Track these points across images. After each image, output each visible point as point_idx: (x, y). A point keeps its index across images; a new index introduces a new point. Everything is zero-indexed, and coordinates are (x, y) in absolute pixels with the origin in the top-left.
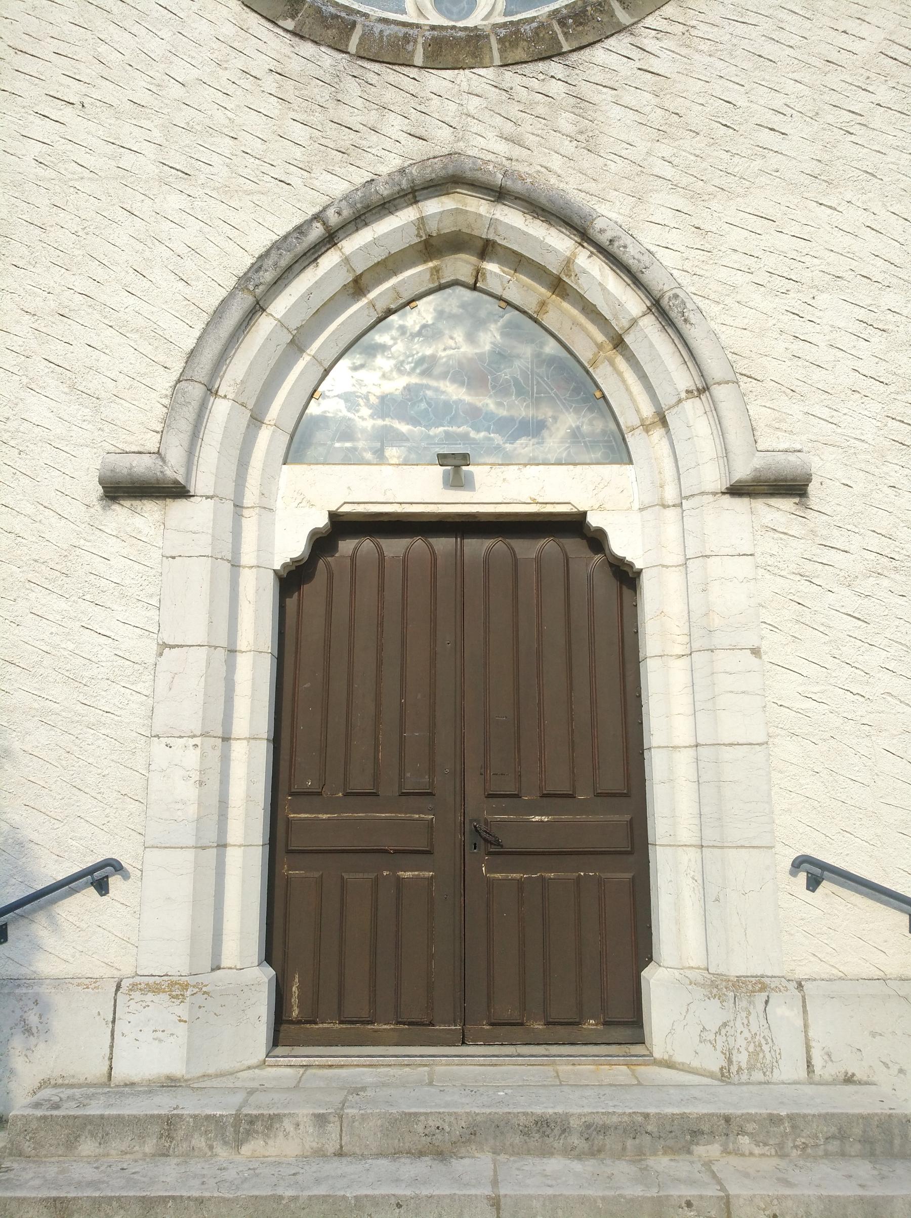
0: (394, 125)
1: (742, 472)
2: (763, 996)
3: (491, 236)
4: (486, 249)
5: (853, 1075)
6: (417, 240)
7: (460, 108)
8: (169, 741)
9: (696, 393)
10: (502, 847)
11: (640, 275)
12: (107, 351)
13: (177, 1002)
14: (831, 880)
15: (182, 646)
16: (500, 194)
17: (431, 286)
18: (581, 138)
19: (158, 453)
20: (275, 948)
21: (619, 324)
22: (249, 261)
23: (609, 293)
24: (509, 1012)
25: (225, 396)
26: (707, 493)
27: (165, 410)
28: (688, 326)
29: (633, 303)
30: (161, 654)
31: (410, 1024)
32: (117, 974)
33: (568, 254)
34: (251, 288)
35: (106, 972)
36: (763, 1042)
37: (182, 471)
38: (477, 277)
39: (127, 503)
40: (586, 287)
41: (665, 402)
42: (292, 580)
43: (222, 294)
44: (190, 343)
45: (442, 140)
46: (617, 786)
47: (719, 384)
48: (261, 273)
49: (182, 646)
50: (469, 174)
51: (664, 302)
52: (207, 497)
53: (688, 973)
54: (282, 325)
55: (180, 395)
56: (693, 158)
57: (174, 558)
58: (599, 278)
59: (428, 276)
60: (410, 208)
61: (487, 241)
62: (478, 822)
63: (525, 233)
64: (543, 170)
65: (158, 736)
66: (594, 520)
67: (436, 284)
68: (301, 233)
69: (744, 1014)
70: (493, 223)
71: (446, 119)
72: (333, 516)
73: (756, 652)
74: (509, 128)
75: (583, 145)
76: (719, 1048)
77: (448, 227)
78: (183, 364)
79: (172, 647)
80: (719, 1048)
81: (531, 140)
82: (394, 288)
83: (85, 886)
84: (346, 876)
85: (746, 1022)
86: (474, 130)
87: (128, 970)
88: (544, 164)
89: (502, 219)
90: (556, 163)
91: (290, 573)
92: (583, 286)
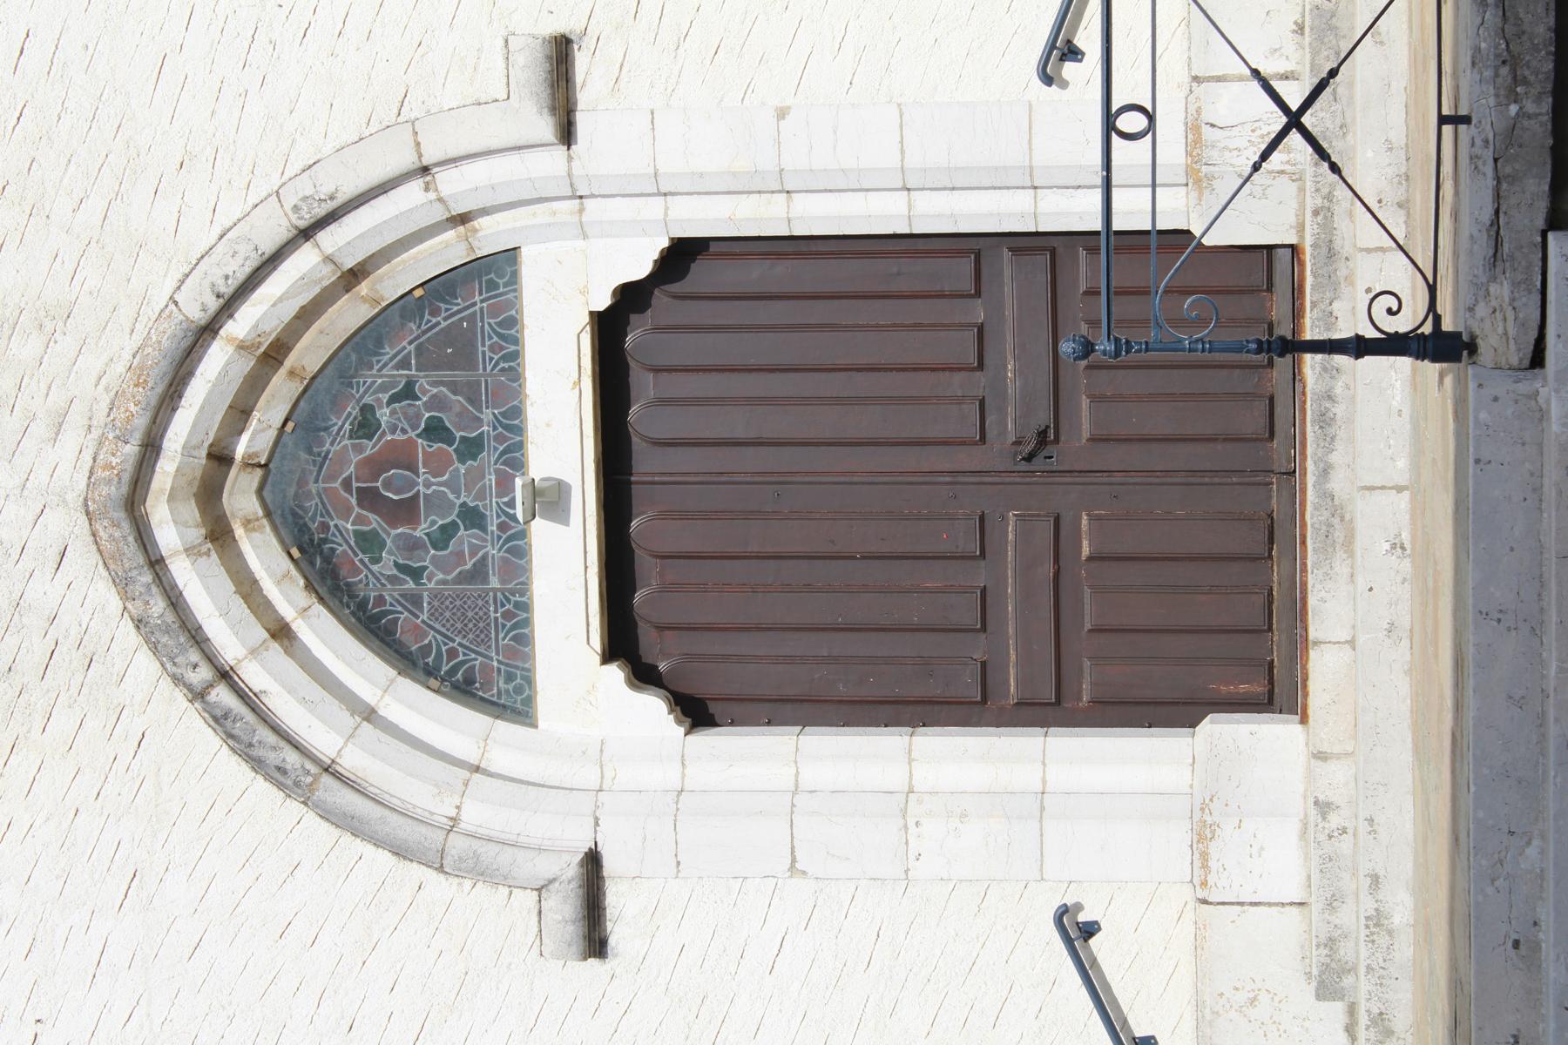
0: (44, 591)
1: (544, 127)
2: (1206, 129)
3: (204, 453)
4: (220, 458)
5: (1296, 23)
6: (214, 555)
7: (12, 498)
8: (912, 857)
9: (429, 178)
10: (1048, 427)
11: (266, 256)
12: (399, 966)
13: (1218, 832)
14: (1074, 27)
15: (793, 848)
16: (151, 447)
17: (268, 529)
18: (49, 326)
19: (539, 890)
20: (1181, 711)
21: (328, 276)
22: (261, 784)
23: (287, 292)
24: (1253, 421)
25: (458, 807)
26: (570, 168)
27: (480, 884)
28: (339, 195)
29: (304, 260)
30: (804, 873)
31: (1271, 541)
32: (1191, 904)
33: (231, 349)
34: (309, 779)
35: (1189, 916)
36: (1258, 133)
37: (566, 857)
38: (253, 465)
39: (609, 925)
40: (275, 323)
41: (439, 214)
42: (696, 712)
43: (311, 818)
44: (384, 856)
45: (66, 524)
46: (966, 266)
47: (420, 156)
48: (288, 767)
49: (793, 848)
50: (125, 490)
51: (303, 224)
52: (597, 824)
53: (1192, 204)
54: (352, 736)
55: (463, 866)
56: (72, 168)
57: (678, 863)
58: (265, 308)
59: (255, 535)
60: (172, 568)
61: (210, 456)
62: (1016, 454)
63: (202, 407)
64: (103, 382)
65: (907, 871)
66: (603, 302)
67: (265, 521)
68: (226, 716)
69: (1227, 154)
70: (188, 449)
71: (31, 518)
72: (608, 656)
73: (782, 113)
74: (39, 429)
75: (61, 324)
76: (1270, 182)
77: (191, 511)
78: (415, 865)
79: (794, 860)
80: (1270, 182)
81: (57, 399)
82: (278, 583)
83: (1088, 949)
84: (1088, 626)
85: (1235, 153)
86: (45, 478)
87: (1187, 893)
88: (94, 381)
89: (182, 441)
90: (91, 363)
91: (685, 713)
92: (273, 327)
